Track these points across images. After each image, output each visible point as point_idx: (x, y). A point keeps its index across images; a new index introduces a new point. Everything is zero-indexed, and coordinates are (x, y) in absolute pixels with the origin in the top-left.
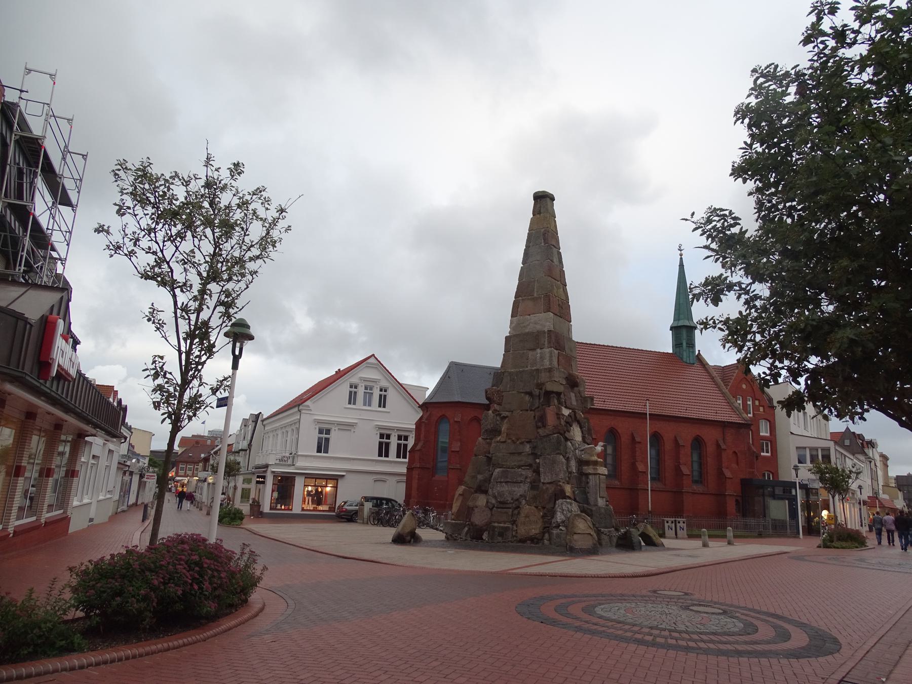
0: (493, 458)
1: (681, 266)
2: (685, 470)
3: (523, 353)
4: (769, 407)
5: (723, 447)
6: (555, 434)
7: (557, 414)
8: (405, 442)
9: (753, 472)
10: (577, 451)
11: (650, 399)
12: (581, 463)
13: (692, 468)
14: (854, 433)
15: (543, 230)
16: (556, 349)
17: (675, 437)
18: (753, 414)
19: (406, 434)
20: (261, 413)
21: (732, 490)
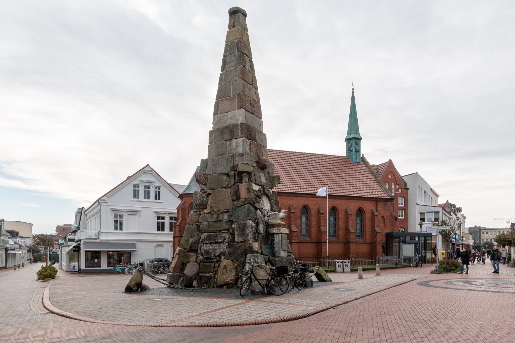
0: (201, 226)
1: (353, 97)
2: (352, 229)
3: (223, 143)
4: (405, 189)
5: (376, 213)
6: (246, 204)
7: (248, 189)
8: (163, 221)
9: (393, 228)
10: (266, 217)
11: (328, 184)
12: (268, 226)
13: (356, 228)
14: (451, 204)
15: (236, 41)
16: (248, 139)
17: (346, 209)
18: (395, 193)
19: (163, 215)
20: (83, 207)
21: (380, 239)
